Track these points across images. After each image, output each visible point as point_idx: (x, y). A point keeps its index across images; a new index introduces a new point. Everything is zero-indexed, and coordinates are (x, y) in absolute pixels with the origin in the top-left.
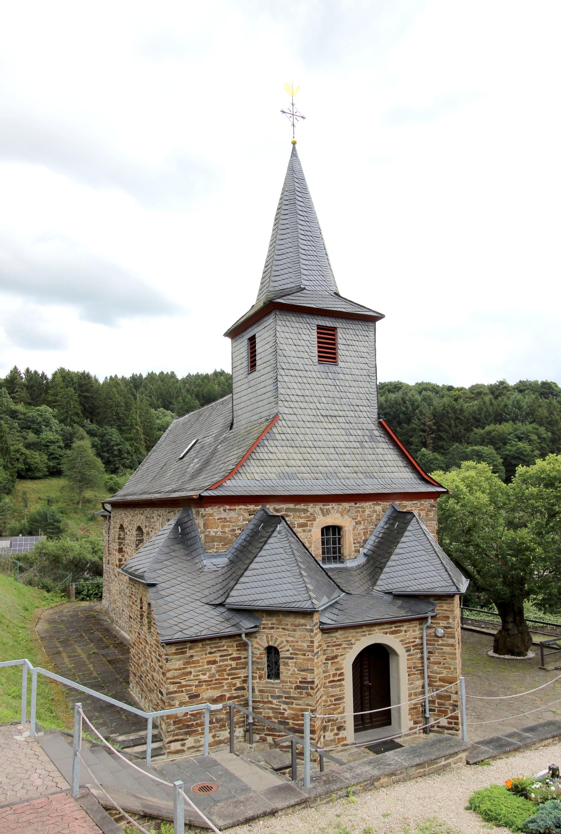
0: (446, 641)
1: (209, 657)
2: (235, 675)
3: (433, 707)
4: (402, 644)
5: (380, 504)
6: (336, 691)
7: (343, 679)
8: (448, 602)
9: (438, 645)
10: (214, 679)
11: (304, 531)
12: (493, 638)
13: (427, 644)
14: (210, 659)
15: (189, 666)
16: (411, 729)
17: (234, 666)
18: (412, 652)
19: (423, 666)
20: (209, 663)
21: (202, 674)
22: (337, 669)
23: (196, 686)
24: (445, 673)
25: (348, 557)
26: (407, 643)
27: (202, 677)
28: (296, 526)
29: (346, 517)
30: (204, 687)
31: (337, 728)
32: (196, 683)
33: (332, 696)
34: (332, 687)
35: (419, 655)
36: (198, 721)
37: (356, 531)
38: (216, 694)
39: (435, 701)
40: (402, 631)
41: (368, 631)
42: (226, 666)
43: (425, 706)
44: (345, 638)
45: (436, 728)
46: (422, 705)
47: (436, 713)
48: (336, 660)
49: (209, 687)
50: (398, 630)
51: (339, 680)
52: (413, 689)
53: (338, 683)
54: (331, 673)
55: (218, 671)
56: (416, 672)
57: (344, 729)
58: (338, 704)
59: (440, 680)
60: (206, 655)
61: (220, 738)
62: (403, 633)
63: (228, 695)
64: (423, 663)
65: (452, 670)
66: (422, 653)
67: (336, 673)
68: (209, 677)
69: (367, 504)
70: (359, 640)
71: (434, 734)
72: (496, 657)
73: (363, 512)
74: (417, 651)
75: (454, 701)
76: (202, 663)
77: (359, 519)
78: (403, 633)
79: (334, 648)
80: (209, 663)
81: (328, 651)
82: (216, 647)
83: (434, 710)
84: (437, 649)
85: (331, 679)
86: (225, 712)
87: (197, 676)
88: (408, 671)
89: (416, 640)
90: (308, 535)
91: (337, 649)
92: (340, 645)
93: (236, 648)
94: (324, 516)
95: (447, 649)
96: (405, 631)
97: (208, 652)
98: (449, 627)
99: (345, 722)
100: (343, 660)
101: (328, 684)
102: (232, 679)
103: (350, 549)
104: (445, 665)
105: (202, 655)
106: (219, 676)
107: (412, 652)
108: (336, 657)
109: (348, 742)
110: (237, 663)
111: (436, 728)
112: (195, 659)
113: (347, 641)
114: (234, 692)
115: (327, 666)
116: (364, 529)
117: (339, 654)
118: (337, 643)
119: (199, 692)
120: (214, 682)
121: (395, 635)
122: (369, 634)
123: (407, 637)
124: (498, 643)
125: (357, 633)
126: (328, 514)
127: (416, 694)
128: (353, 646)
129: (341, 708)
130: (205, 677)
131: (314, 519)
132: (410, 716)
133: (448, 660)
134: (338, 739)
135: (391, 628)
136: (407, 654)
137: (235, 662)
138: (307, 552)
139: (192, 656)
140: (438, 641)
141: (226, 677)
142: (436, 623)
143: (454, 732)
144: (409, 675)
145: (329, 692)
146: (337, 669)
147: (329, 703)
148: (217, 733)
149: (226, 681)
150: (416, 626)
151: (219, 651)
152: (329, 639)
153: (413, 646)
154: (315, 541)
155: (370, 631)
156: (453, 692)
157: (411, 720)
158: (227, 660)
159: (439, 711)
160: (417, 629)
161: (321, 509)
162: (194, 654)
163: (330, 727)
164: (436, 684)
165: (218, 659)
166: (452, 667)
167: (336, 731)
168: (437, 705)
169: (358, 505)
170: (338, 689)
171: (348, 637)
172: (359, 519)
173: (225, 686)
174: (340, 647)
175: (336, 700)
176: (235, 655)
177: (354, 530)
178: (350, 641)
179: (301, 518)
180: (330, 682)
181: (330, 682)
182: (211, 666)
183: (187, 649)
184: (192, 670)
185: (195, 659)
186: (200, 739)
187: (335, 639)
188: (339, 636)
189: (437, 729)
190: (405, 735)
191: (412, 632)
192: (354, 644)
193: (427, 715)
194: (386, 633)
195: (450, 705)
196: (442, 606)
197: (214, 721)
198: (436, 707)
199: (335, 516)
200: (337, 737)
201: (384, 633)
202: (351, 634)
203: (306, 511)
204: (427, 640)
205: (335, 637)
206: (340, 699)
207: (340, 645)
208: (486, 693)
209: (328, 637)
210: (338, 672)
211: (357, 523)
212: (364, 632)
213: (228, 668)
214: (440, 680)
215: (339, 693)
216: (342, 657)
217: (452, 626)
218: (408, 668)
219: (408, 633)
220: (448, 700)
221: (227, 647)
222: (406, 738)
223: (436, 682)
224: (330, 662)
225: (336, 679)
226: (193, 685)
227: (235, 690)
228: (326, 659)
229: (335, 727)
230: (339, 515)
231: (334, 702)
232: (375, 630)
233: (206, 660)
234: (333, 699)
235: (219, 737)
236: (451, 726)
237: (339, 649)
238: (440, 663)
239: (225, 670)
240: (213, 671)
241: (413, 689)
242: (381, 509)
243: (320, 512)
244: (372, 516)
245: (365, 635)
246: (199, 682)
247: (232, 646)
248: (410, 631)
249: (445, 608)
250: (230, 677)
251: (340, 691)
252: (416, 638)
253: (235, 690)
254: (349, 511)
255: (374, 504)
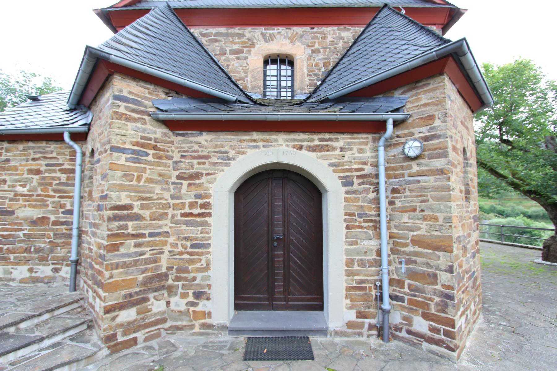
0: (426, 165)
1: (32, 165)
2: (65, 192)
3: (399, 292)
4: (334, 171)
5: (349, 30)
6: (195, 232)
7: (209, 215)
8: (431, 87)
9: (409, 176)
10: (35, 194)
11: (238, 58)
12: (541, 252)
13: (388, 177)
14: (33, 167)
15: (3, 172)
16: (350, 325)
17: (64, 180)
18: (355, 187)
19: (379, 215)
20: (31, 172)
21: (21, 185)
22: (198, 196)
23: (11, 200)
24: (423, 229)
25: (299, 91)
26: (344, 171)
27: (20, 189)
28: (228, 52)
29: (298, 43)
30: (21, 202)
31: (194, 294)
32: (11, 195)
33: (185, 238)
34: (187, 224)
35: (372, 195)
36: (10, 246)
37: (312, 62)
38: (36, 213)
39: (403, 282)
40: (334, 149)
41: (263, 140)
42: (53, 178)
43: (381, 287)
44: (217, 146)
45: (404, 334)
46: (375, 285)
47: (406, 304)
48: (197, 181)
49: (27, 203)
50: (327, 145)
51: (199, 215)
52: (357, 252)
53: (199, 219)
54: (187, 201)
55: (40, 184)
56: (365, 225)
57: (208, 299)
58: (197, 254)
59: (415, 242)
60: (27, 161)
61: (38, 275)
62: (338, 152)
63: (53, 218)
64: (378, 209)
65: (441, 222)
66: (377, 191)
67: (197, 203)
68: (29, 191)
69: (330, 29)
70: (244, 153)
71: (401, 344)
72: (546, 264)
73: (324, 38)
74: (368, 186)
75: (442, 285)
76: (21, 170)
77: (317, 46)
78: (338, 152)
79: (195, 162)
80: (31, 172)
81: (183, 165)
82: (41, 153)
83: (402, 300)
84: (408, 182)
85: (187, 210)
86: (48, 240)
87: (13, 186)
88: (345, 220)
89: (365, 167)
90: (243, 63)
91: (199, 164)
92: (207, 157)
93: (68, 157)
94: (266, 42)
95: (430, 181)
96: (342, 149)
97: (30, 158)
98: (434, 137)
99: (209, 286)
100: (211, 182)
101: (179, 218)
102: (59, 197)
103: (302, 81)
104: (425, 213)
105: (22, 160)
106: (42, 190)
107: (355, 187)
108: (197, 176)
109: (215, 321)
110: (68, 177)
111: (404, 334)
112: (12, 164)
113: (220, 152)
114: (61, 215)
115: (180, 189)
116: (323, 59)
117: (204, 172)
118: (200, 154)
119: (13, 208)
120: (34, 197)
121: (320, 154)
122: (264, 146)
123: (346, 159)
124: (548, 250)
125: (241, 141)
126: (272, 40)
127: (362, 263)
128: (232, 162)
129: (203, 262)
130: (25, 189)
131: (253, 45)
132: (348, 301)
133: (431, 201)
134: (194, 312)
135: (312, 140)
136: (344, 189)
137: (65, 176)
138: (200, 48)
139: (8, 160)
140: (411, 168)
141: (52, 193)
142: (406, 135)
143: (442, 350)
144: (348, 227)
145: (181, 232)
146: (198, 196)
147: (181, 249)
148: (34, 267)
149: (51, 200)
150: (366, 143)
151: (46, 158)
152: (186, 145)
153: (358, 177)
154: (253, 71)
155: (267, 141)
156: (443, 267)
157: (351, 308)
158: (55, 171)
159: (411, 302)
160: (368, 148)
161: (262, 34)
162: (11, 158)
163: (180, 290)
164: (406, 249)
165: (43, 168)
166: (441, 216)
167: (191, 299)
168: (406, 290)
169: (315, 30)
170: (200, 228)
171: (222, 146)
172: (317, 46)
173: (50, 206)
174: (207, 161)
175: (192, 246)
176: (66, 166)
177: (309, 58)
178: (226, 152)
179: (235, 43)
180: (183, 215)
181: (183, 215)
182: (33, 176)
183: (3, 151)
184: (7, 178)
185: (12, 164)
186: (11, 270)
187: (196, 147)
188: (204, 143)
189: (407, 336)
190: (336, 333)
191: (357, 150)
192: (234, 159)
193: (386, 305)
194: (301, 148)
195: (435, 294)
196: (418, 100)
197: (32, 250)
198: (404, 293)
199: (282, 40)
200: (192, 309)
201: (294, 146)
202: (227, 140)
203: (242, 35)
204: (387, 169)
205: (197, 143)
206: (201, 245)
207: (207, 157)
208: (531, 296)
209: (183, 142)
210: (200, 201)
211: (313, 52)
212: (255, 141)
213: (55, 182)
214: (415, 242)
215: (199, 235)
216: (209, 177)
217: (441, 133)
218: (346, 214)
219: (348, 154)
220: (432, 284)
221: (58, 154)
222: (338, 339)
223: (406, 245)
224: (185, 183)
225: (196, 211)
226: (6, 198)
227: (63, 213)
228: (178, 177)
229: (191, 292)
230: (287, 41)
231: (189, 250)
232: (276, 141)
233: (26, 168)
234: (189, 244)
235: (36, 272)
236: (437, 336)
237: (204, 163)
238: (414, 210)
239: (51, 184)
240: (35, 183)
241: (357, 252)
242: (351, 35)
243: (261, 37)
244: (337, 44)
245: (257, 147)
246: (15, 195)
247: (64, 154)
248: (351, 149)
249: (424, 101)
250: (58, 195)
251: (202, 233)
252: (366, 164)
253: (63, 213)
254: (302, 36)
255: (339, 30)
